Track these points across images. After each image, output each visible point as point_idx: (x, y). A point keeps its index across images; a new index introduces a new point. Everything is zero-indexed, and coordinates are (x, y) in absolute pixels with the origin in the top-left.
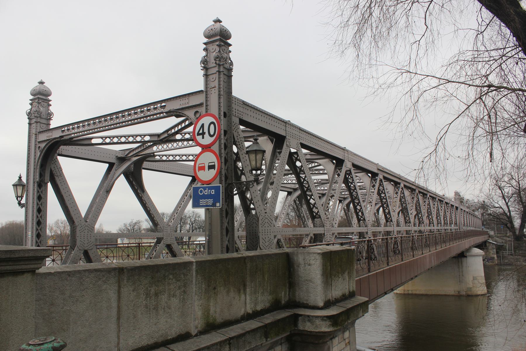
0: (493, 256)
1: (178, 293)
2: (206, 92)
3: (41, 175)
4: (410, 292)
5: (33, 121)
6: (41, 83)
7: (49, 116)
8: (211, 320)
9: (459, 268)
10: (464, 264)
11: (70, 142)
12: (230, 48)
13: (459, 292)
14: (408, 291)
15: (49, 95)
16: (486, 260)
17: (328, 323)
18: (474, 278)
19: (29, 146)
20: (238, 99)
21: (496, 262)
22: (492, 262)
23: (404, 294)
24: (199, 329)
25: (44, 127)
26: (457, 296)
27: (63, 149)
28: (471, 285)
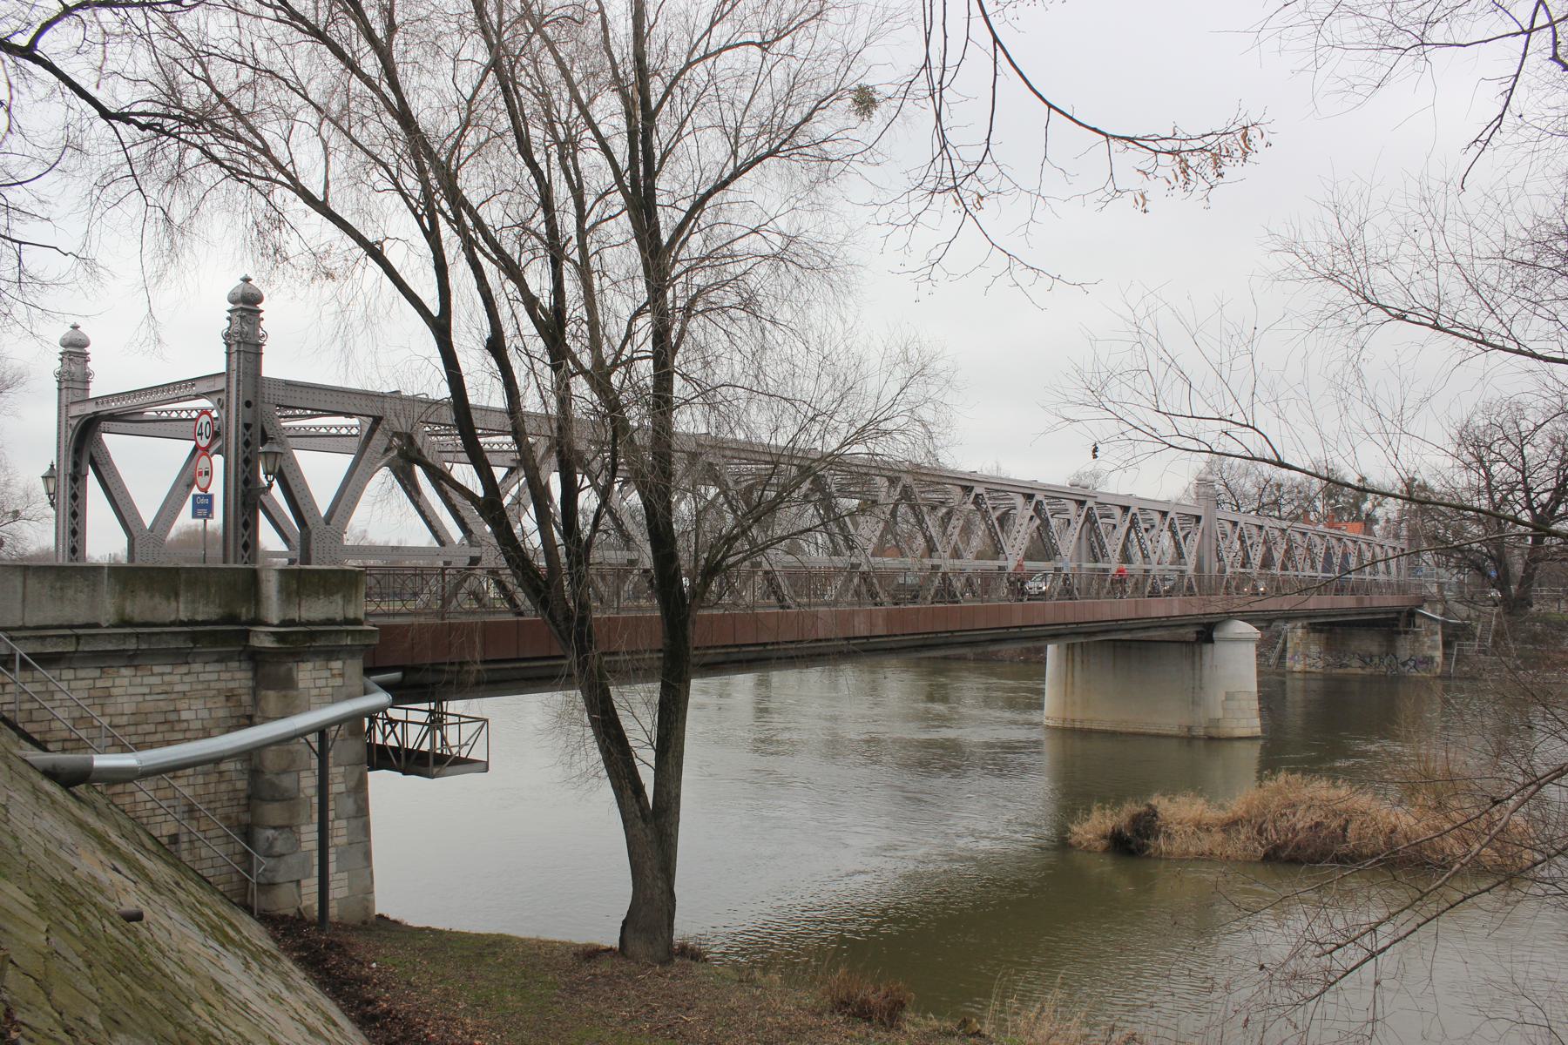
0: (1430, 653)
1: (86, 590)
2: (227, 375)
3: (76, 465)
4: (1078, 725)
5: (64, 385)
6: (75, 327)
7: (85, 379)
8: (127, 618)
9: (1193, 669)
10: (1207, 659)
11: (113, 417)
12: (262, 315)
13: (1190, 729)
14: (1073, 720)
15: (87, 345)
16: (1412, 664)
17: (272, 638)
18: (1229, 696)
19: (59, 422)
20: (275, 380)
21: (1439, 671)
22: (1424, 670)
23: (1064, 730)
24: (111, 622)
25: (79, 396)
26: (1182, 737)
27: (104, 425)
28: (1219, 714)
